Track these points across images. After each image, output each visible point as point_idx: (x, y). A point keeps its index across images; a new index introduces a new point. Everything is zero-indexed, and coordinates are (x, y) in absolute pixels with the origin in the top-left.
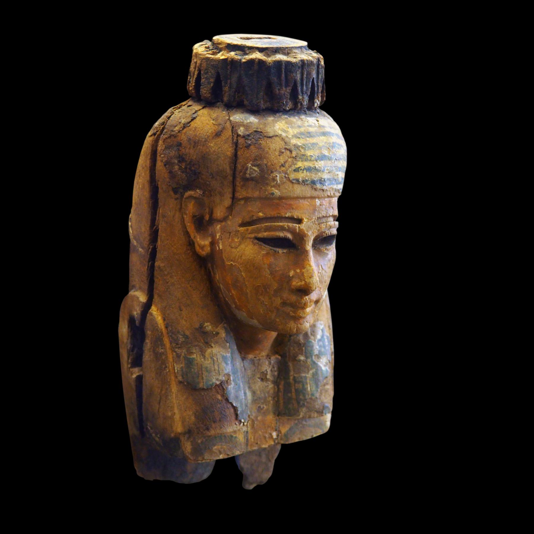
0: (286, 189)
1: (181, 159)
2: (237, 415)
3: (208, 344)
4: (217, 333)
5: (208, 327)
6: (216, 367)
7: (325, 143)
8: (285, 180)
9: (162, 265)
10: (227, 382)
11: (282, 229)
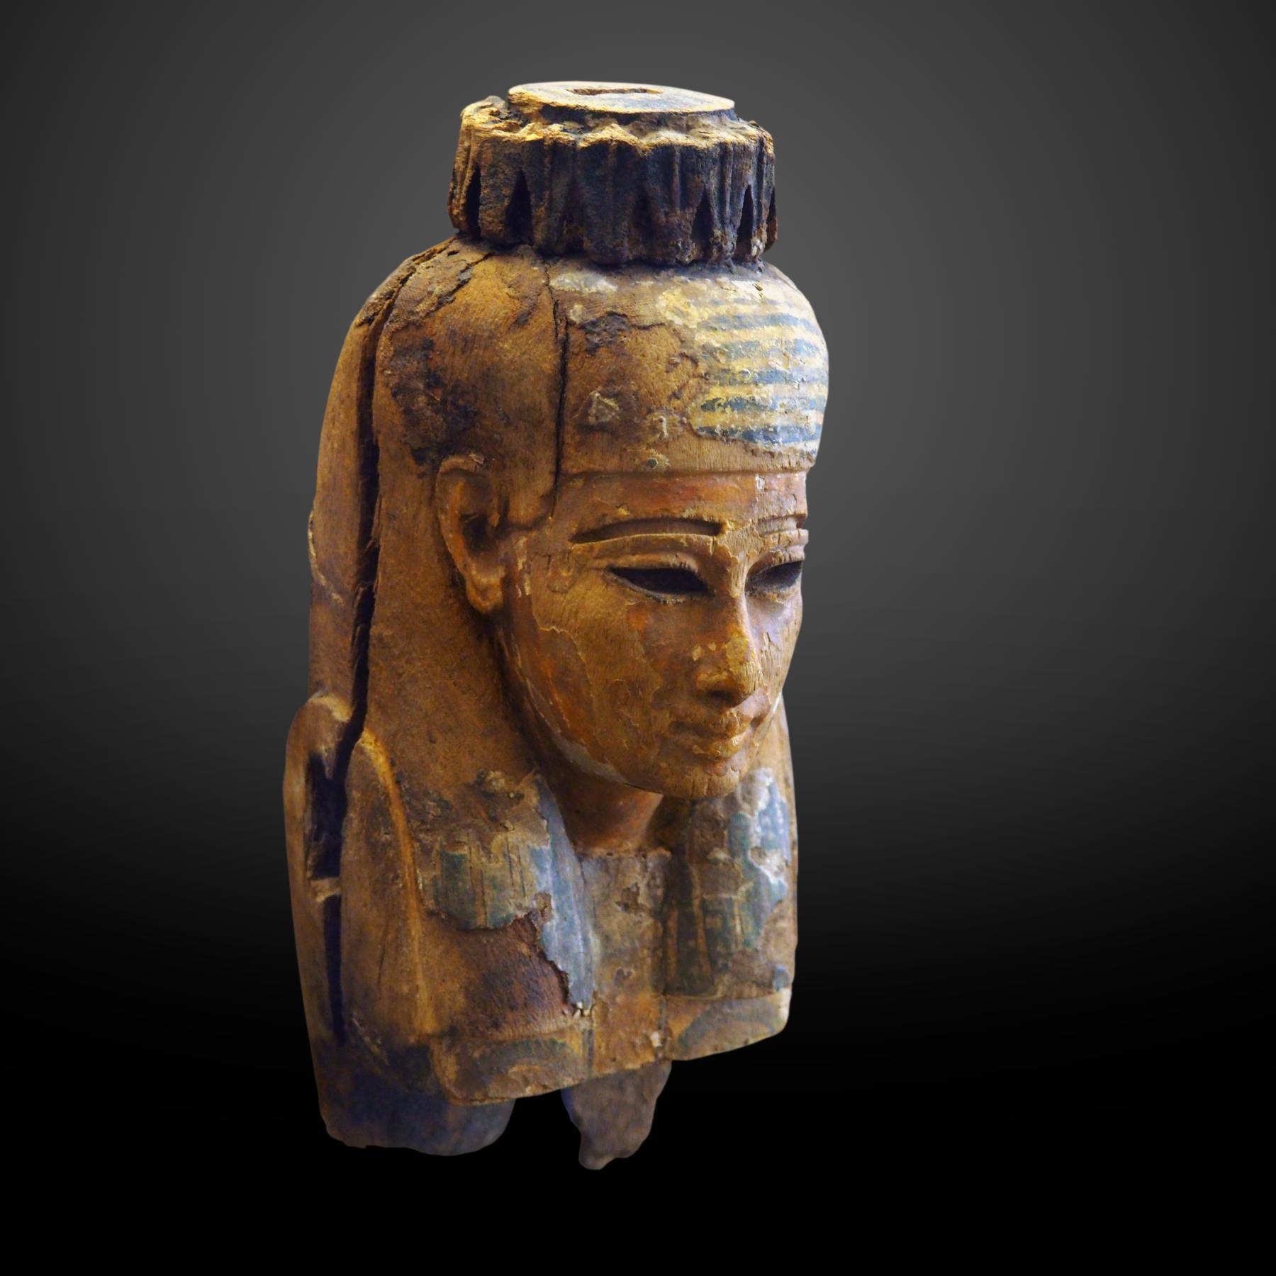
0: (683, 451)
1: (433, 380)
2: (565, 992)
3: (497, 823)
4: (520, 797)
5: (498, 780)
6: (517, 878)
7: (777, 341)
8: (680, 429)
9: (387, 633)
10: (544, 912)
11: (675, 547)
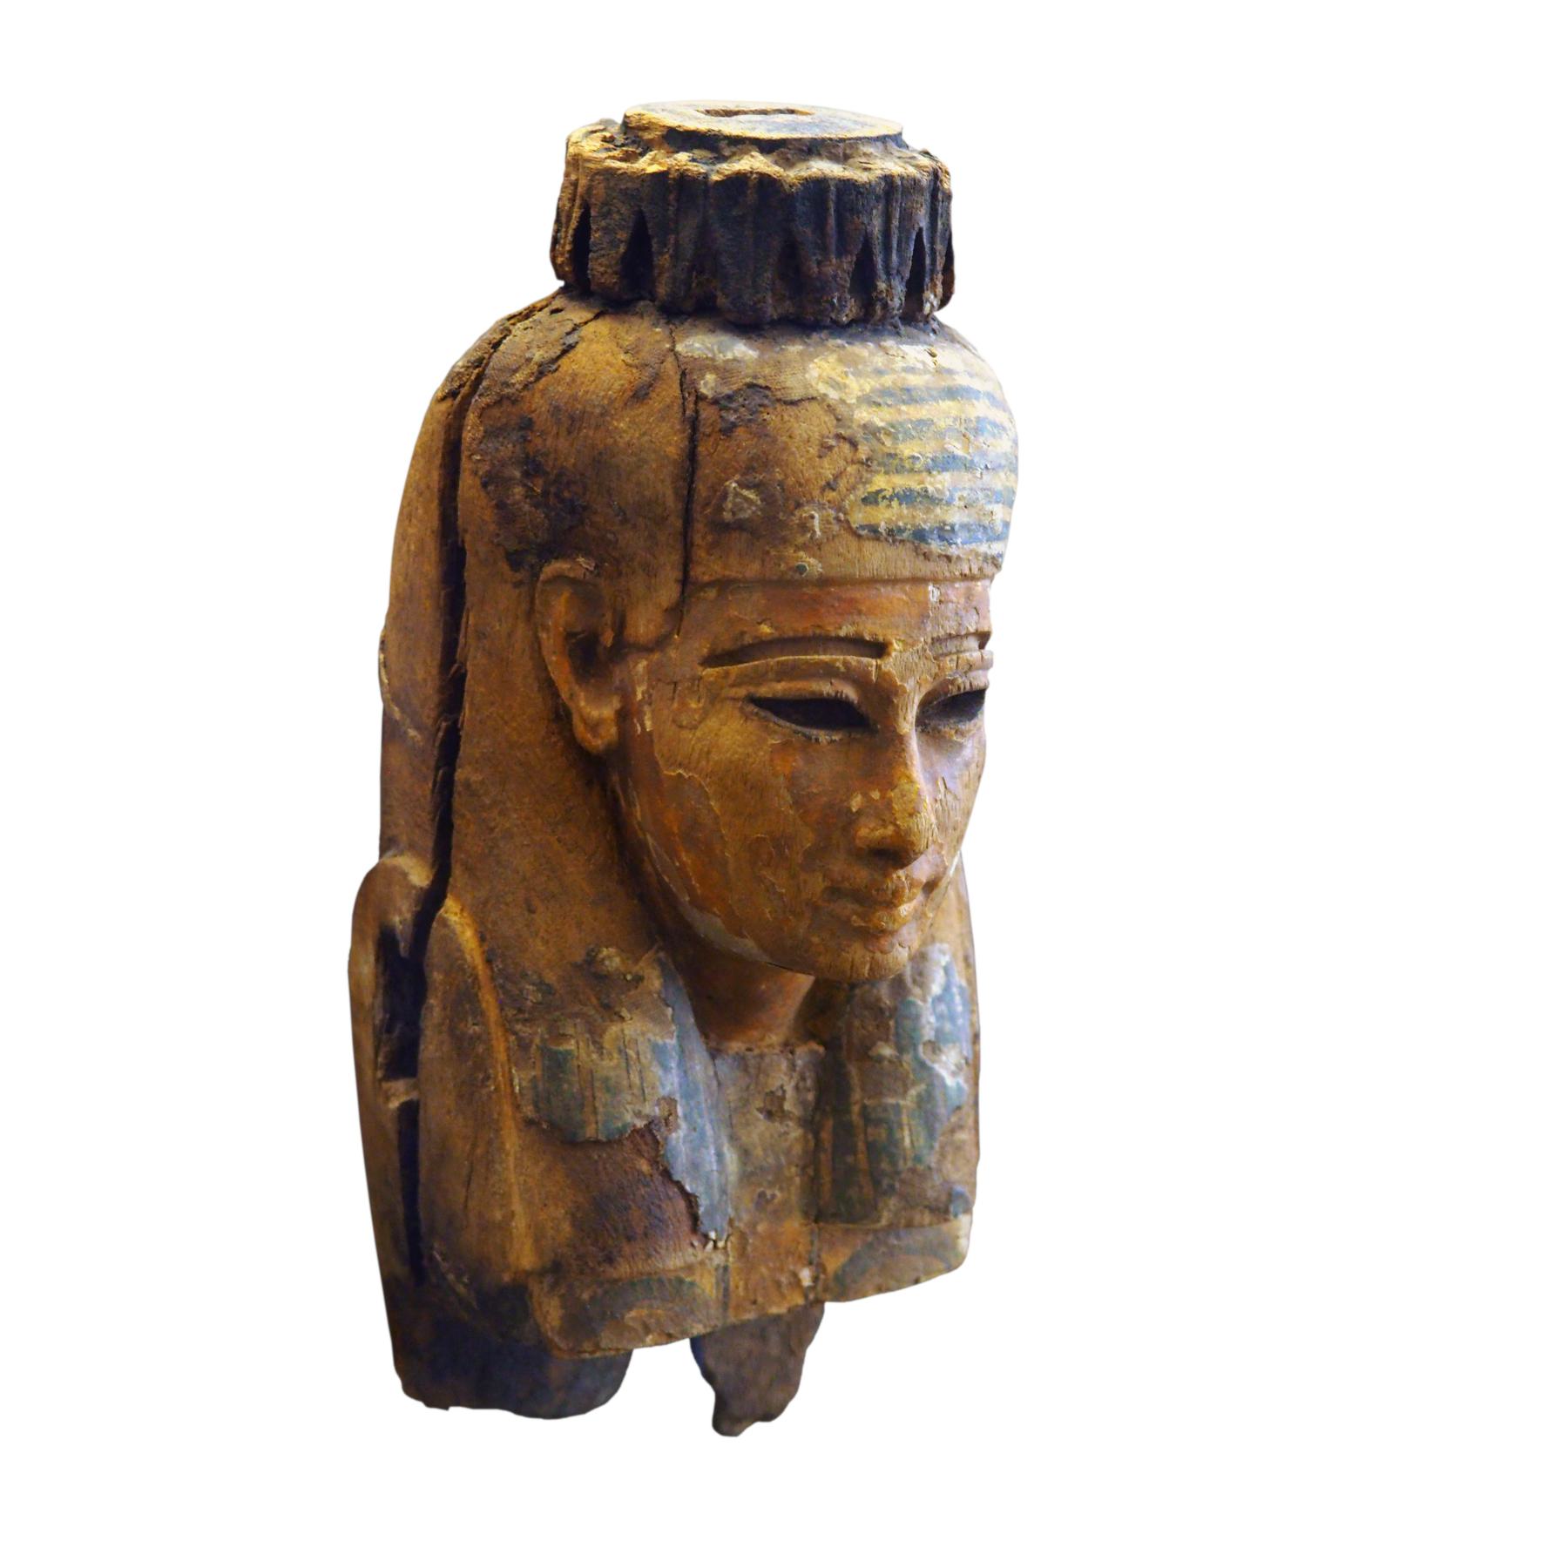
0: (839, 555)
1: (532, 466)
2: (695, 1219)
3: (610, 1011)
4: (639, 979)
5: (612, 959)
6: (635, 1079)
7: (955, 419)
8: (836, 528)
9: (475, 778)
10: (668, 1121)
11: (829, 672)
